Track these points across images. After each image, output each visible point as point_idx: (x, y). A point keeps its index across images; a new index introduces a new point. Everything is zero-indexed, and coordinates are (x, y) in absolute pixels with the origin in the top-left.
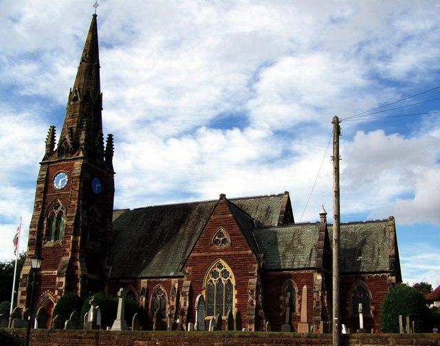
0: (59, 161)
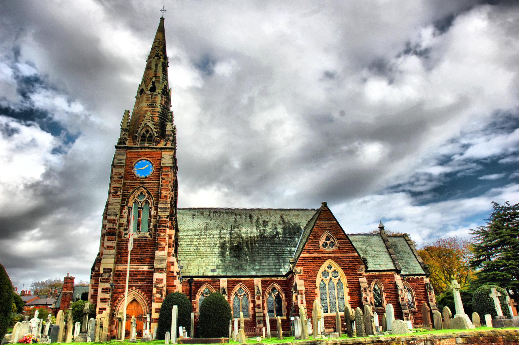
0: (141, 148)
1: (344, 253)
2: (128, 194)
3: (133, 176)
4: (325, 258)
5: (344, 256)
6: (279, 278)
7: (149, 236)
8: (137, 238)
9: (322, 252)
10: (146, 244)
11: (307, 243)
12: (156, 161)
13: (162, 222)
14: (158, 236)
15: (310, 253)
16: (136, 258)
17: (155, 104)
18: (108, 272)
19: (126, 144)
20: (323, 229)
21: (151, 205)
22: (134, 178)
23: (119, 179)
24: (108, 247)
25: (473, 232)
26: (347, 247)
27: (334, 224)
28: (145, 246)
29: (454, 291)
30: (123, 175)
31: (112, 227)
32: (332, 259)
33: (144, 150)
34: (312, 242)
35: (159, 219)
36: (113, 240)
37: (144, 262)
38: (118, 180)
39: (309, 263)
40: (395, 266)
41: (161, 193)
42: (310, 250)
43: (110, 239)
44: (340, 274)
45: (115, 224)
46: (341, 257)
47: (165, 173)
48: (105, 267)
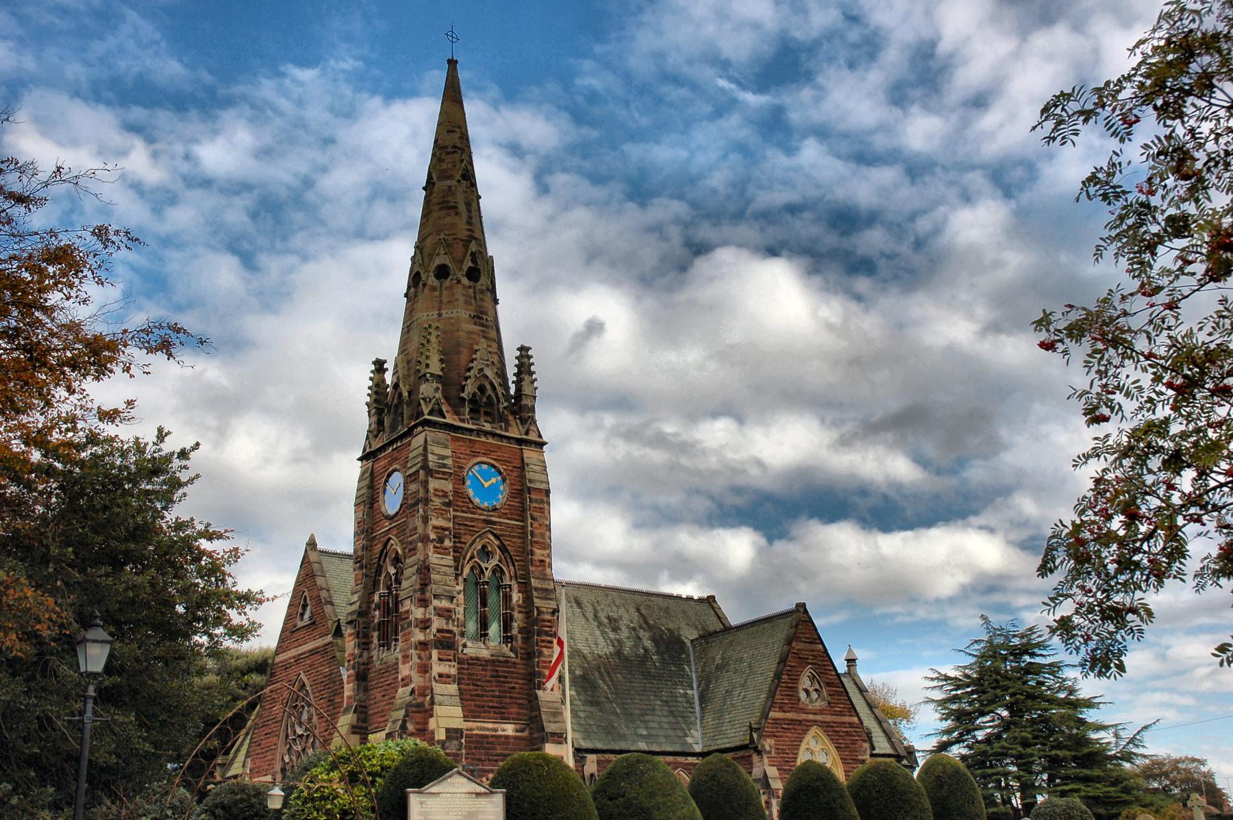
1: (837, 715)
2: (463, 546)
3: (467, 503)
4: (808, 724)
5: (838, 721)
6: (689, 758)
7: (512, 655)
8: (489, 657)
9: (804, 711)
10: (508, 672)
11: (779, 689)
12: (511, 471)
13: (544, 623)
14: (538, 657)
15: (784, 711)
16: (491, 704)
17: (485, 317)
18: (457, 738)
19: (445, 418)
20: (803, 662)
21: (508, 579)
22: (469, 507)
23: (445, 508)
24: (441, 675)
25: (936, 675)
26: (841, 704)
27: (819, 651)
28: (506, 677)
29: (1196, 809)
30: (451, 498)
31: (445, 628)
32: (820, 726)
33: (483, 439)
34: (787, 687)
35: (538, 615)
36: (450, 661)
37: (506, 715)
38: (443, 510)
39: (784, 732)
40: (402, 708)
41: (532, 553)
42: (785, 703)
43: (445, 657)
44: (832, 759)
45: (450, 621)
46: (834, 723)
47: (536, 505)
48: (450, 726)
